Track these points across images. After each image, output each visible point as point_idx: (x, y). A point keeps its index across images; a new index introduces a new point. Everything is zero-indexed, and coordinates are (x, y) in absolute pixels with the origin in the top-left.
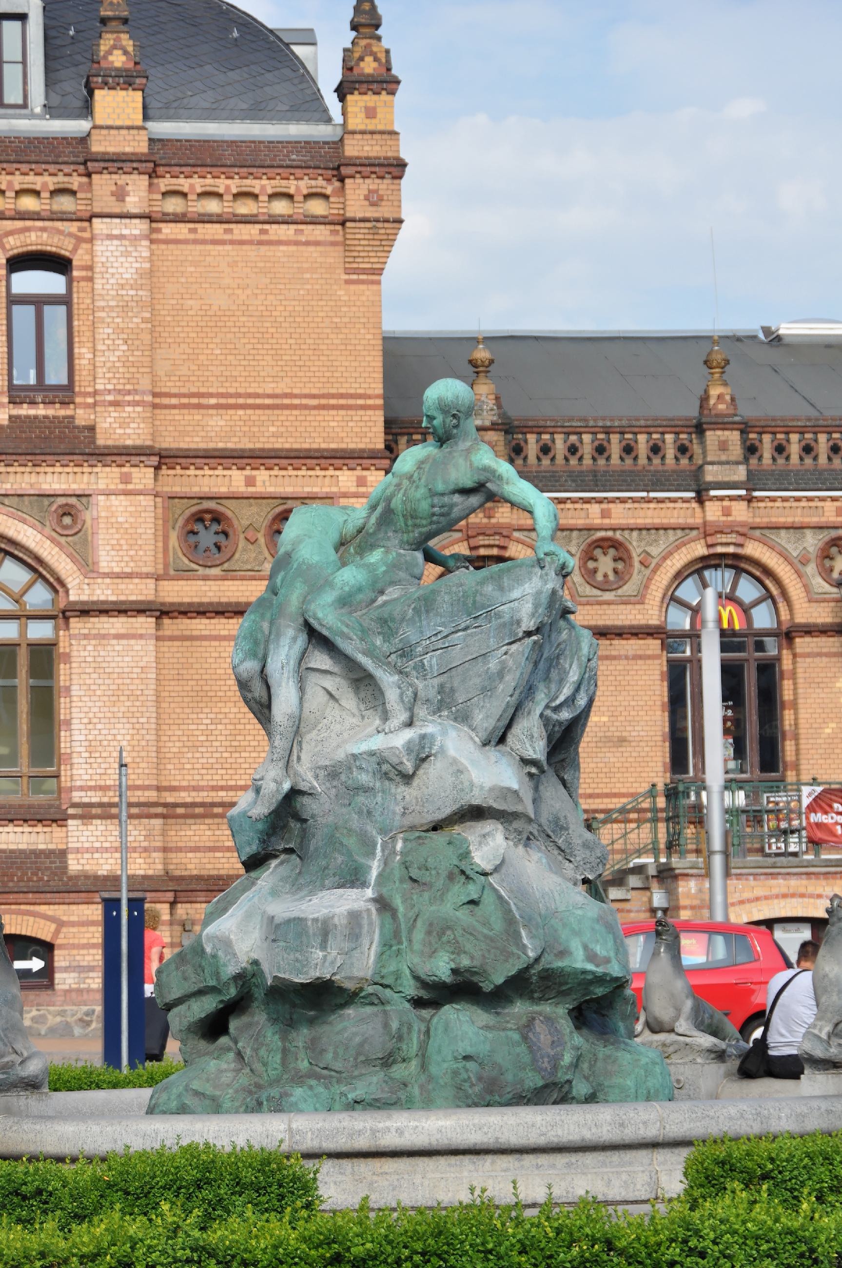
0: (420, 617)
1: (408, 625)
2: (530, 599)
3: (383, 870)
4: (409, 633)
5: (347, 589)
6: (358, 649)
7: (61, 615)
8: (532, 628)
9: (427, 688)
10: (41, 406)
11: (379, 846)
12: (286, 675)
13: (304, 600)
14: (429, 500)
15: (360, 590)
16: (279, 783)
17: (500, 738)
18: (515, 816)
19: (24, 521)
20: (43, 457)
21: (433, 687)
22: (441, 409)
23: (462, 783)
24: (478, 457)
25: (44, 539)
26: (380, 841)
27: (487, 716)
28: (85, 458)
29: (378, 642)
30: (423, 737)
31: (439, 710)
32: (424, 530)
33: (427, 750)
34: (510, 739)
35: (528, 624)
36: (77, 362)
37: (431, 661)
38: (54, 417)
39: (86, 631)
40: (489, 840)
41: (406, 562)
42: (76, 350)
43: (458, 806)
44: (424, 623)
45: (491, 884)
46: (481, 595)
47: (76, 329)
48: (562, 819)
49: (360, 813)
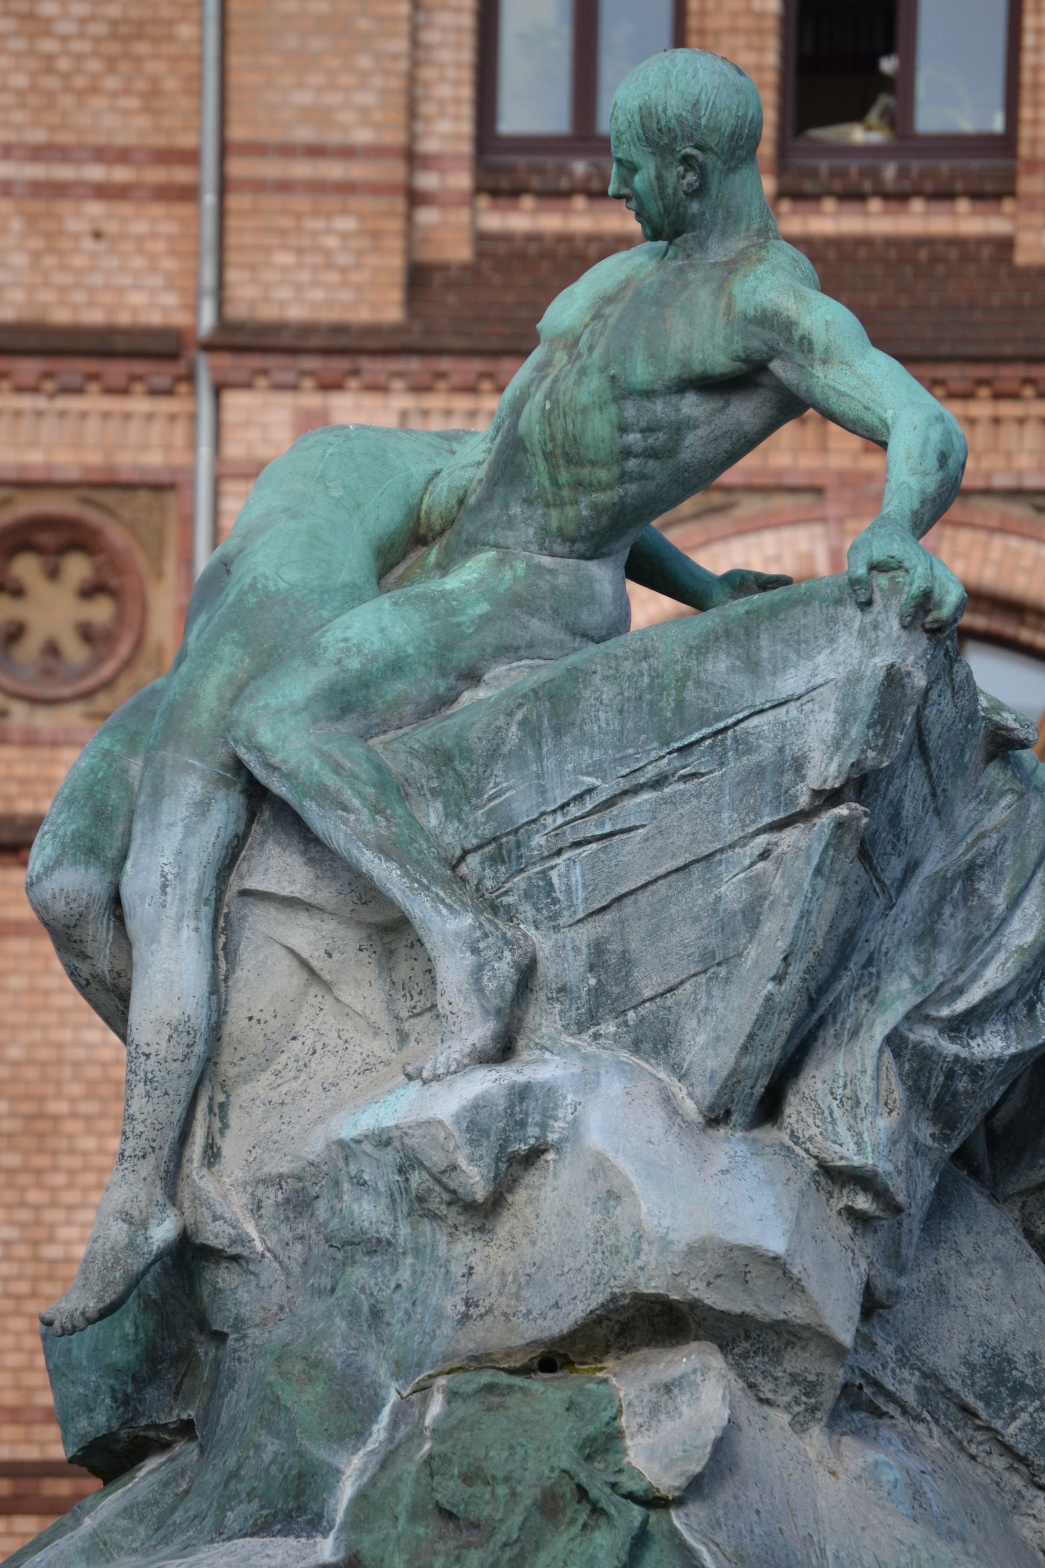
1: (507, 770)
2: (830, 696)
3: (373, 1482)
4: (515, 794)
5: (354, 664)
6: (362, 836)
9: (562, 954)
11: (386, 1411)
12: (172, 910)
13: (238, 692)
14: (612, 410)
15: (396, 667)
16: (138, 1224)
17: (762, 1099)
18: (785, 1335)
21: (576, 950)
22: (649, 142)
23: (616, 1229)
26: (393, 1397)
27: (718, 1034)
29: (432, 816)
30: (521, 1093)
31: (593, 1018)
32: (603, 497)
33: (532, 1131)
34: (794, 1109)
35: (825, 770)
37: (570, 874)
40: (682, 1399)
41: (554, 588)
43: (599, 1299)
44: (550, 764)
45: (674, 1533)
46: (698, 683)
48: (1021, 1361)
49: (353, 1313)
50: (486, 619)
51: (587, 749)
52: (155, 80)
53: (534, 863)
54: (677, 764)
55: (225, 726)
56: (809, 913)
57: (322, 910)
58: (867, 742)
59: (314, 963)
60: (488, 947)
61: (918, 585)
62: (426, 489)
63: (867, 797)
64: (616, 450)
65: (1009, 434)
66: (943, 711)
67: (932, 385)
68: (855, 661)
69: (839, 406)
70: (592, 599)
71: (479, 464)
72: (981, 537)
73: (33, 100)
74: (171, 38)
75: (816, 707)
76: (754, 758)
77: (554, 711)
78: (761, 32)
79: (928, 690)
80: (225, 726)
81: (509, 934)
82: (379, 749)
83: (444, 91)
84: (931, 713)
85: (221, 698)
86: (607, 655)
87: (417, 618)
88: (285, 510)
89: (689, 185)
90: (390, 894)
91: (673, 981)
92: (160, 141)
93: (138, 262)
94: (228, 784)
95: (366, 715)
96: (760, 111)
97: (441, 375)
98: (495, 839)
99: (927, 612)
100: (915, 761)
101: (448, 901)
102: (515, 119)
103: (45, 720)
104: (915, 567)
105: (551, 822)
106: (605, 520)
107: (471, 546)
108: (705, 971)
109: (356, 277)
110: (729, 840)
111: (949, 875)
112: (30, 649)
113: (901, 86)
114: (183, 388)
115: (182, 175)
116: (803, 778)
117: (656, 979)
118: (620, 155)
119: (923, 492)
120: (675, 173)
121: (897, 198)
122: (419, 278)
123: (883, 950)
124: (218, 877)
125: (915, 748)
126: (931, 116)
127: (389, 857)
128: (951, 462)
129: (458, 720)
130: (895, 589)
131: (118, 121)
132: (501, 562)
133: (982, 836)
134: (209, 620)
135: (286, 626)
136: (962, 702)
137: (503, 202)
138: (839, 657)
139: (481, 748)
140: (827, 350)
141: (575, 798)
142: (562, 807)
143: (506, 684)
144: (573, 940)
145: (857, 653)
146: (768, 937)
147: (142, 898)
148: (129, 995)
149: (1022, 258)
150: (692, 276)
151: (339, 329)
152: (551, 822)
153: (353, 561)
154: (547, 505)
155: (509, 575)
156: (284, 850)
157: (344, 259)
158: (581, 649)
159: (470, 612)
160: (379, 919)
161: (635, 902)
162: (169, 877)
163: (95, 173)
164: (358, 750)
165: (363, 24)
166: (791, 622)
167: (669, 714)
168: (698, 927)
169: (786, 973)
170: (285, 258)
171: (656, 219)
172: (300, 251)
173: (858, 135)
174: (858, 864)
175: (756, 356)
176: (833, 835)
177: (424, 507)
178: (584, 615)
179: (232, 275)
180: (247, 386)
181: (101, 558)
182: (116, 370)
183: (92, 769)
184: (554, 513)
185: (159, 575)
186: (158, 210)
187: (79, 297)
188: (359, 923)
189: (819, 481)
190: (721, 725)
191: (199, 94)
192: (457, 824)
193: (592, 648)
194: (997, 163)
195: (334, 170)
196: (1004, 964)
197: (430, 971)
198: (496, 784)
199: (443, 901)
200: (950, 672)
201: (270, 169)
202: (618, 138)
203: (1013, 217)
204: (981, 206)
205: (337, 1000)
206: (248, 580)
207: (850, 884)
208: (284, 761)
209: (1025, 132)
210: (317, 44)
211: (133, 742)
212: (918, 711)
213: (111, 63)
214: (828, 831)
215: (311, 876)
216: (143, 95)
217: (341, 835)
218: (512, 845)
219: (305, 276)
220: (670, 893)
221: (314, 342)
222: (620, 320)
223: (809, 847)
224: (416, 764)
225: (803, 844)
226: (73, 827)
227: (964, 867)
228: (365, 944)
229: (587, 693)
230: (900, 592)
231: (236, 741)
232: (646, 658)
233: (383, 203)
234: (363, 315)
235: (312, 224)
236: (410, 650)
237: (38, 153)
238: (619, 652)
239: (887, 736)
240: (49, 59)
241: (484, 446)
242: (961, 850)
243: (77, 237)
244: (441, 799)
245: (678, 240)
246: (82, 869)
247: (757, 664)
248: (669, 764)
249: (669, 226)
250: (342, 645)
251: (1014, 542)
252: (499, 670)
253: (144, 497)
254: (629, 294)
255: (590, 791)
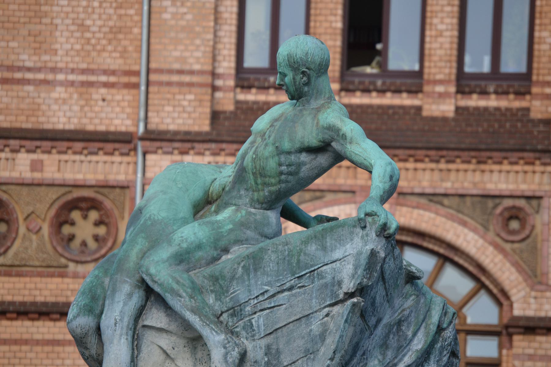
0: (249, 275)
1: (238, 283)
2: (351, 260)
4: (240, 292)
5: (185, 245)
7: (504, 332)
8: (352, 290)
10: (493, 96)
12: (118, 332)
13: (143, 255)
14: (277, 158)
15: (199, 247)
19: (464, 224)
20: (488, 154)
21: (261, 348)
22: (290, 66)
24: (325, 115)
25: (486, 245)
28: (537, 155)
29: (211, 299)
32: (273, 189)
35: (349, 285)
36: (536, 47)
37: (259, 321)
38: (507, 109)
39: (531, 351)
41: (255, 220)
42: (537, 34)
44: (252, 282)
46: (305, 254)
47: (538, 9)
50: (231, 230)
51: (266, 276)
52: (125, 47)
53: (246, 317)
54: (297, 282)
55: (139, 267)
56: (343, 336)
57: (171, 332)
58: (364, 276)
59: (168, 352)
60: (230, 346)
61: (382, 221)
62: (211, 185)
63: (364, 295)
64: (278, 172)
65: (420, 174)
66: (390, 265)
67: (393, 156)
68: (360, 247)
69: (356, 158)
70: (268, 224)
71: (230, 176)
72: (410, 209)
73: (83, 54)
74: (131, 33)
75: (346, 263)
76: (324, 281)
77: (254, 263)
78: (335, 34)
79: (385, 258)
80: (139, 267)
81: (237, 342)
82: (193, 275)
83: (225, 52)
84: (386, 266)
85: (137, 257)
86: (273, 244)
87: (207, 230)
88: (162, 191)
89: (304, 81)
90: (195, 327)
91: (294, 359)
92: (127, 68)
93: (118, 109)
94: (139, 287)
95: (188, 263)
96: (329, 56)
97: (223, 150)
98: (233, 308)
99: (385, 231)
100: (381, 283)
101: (216, 330)
102: (249, 62)
103: (81, 269)
104: (381, 215)
105: (253, 302)
106: (273, 197)
107: (227, 205)
108: (306, 356)
109: (193, 115)
110: (315, 310)
111: (392, 324)
112: (76, 243)
113: (384, 54)
114: (132, 153)
115: (134, 79)
116: (341, 288)
117: (289, 359)
118: (280, 71)
119: (384, 189)
120: (299, 77)
121: (382, 92)
122: (215, 116)
123: (369, 350)
124: (135, 321)
125: (381, 278)
126: (393, 64)
127: (195, 314)
128: (394, 179)
129: (221, 266)
130: (374, 222)
131: (111, 61)
132: (237, 210)
133: (404, 310)
134: (134, 229)
135: (161, 232)
136: (397, 263)
137: (245, 90)
138: (354, 246)
139: (228, 275)
140: (351, 139)
141: (261, 294)
142: (257, 297)
143: (238, 253)
144: (260, 344)
145: (361, 245)
146: (328, 345)
147: (108, 328)
148: (102, 362)
149: (425, 113)
150: (305, 112)
151: (187, 133)
152: (253, 302)
153: (185, 209)
154: (253, 191)
155: (239, 215)
156: (158, 311)
157: (189, 109)
158: (264, 241)
159: (226, 228)
160: (191, 336)
161: (282, 331)
162: (118, 320)
163: (103, 78)
164: (185, 276)
165: (198, 29)
166: (337, 233)
167: (294, 265)
168: (303, 341)
169: (334, 357)
170: (169, 109)
171: (292, 92)
172: (174, 106)
173: (368, 70)
174: (360, 319)
175: (327, 141)
176: (351, 308)
177: (210, 191)
178: (266, 229)
179: (150, 114)
180: (155, 152)
181: (102, 213)
182: (109, 147)
183: (91, 282)
184: (256, 194)
185: (123, 218)
186: (125, 91)
187: (97, 121)
188: (184, 337)
189: (354, 189)
190: (313, 269)
191: (140, 52)
192: (219, 302)
193: (268, 241)
194: (417, 81)
195: (187, 79)
196: (411, 356)
197: (209, 355)
198: (234, 289)
199: (214, 330)
200: (393, 252)
201: (165, 78)
202: (280, 65)
203: (422, 99)
204: (411, 95)
205: (176, 365)
206: (148, 216)
207: (357, 326)
208: (159, 279)
209: (426, 71)
210: (182, 35)
211: (106, 272)
212: (382, 265)
213: (110, 42)
214: (349, 307)
215: (168, 320)
216: (120, 52)
217: (179, 306)
218: (239, 310)
219: (176, 115)
220: (294, 328)
221: (178, 137)
222: (280, 127)
223: (343, 313)
224: (206, 281)
225: (341, 311)
226: (84, 302)
227: (397, 321)
228: (186, 345)
229: (266, 257)
230: (376, 223)
231: (142, 272)
232: (287, 245)
233: (204, 90)
234: (196, 128)
235: (178, 97)
236: (204, 241)
237: (84, 72)
238: (278, 242)
239: (371, 274)
240: (89, 39)
241: (232, 170)
242: (396, 315)
243: (96, 101)
244: (214, 294)
245: (300, 100)
246: (87, 317)
247: (325, 248)
248: (294, 282)
249: (297, 95)
250: (180, 239)
251: (421, 212)
252: (236, 248)
253: (118, 190)
254: (283, 118)
255: (266, 291)
